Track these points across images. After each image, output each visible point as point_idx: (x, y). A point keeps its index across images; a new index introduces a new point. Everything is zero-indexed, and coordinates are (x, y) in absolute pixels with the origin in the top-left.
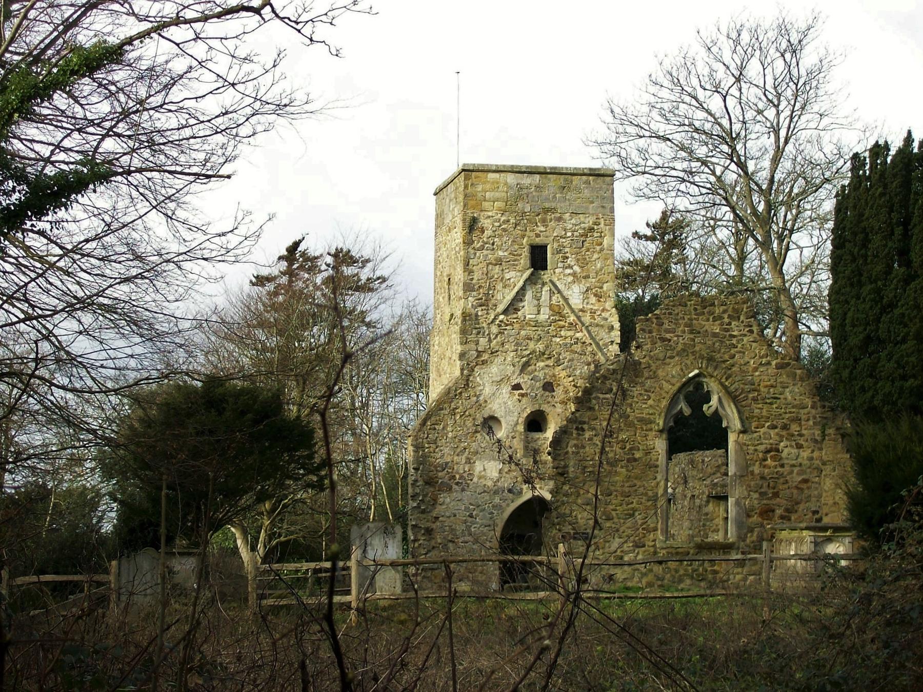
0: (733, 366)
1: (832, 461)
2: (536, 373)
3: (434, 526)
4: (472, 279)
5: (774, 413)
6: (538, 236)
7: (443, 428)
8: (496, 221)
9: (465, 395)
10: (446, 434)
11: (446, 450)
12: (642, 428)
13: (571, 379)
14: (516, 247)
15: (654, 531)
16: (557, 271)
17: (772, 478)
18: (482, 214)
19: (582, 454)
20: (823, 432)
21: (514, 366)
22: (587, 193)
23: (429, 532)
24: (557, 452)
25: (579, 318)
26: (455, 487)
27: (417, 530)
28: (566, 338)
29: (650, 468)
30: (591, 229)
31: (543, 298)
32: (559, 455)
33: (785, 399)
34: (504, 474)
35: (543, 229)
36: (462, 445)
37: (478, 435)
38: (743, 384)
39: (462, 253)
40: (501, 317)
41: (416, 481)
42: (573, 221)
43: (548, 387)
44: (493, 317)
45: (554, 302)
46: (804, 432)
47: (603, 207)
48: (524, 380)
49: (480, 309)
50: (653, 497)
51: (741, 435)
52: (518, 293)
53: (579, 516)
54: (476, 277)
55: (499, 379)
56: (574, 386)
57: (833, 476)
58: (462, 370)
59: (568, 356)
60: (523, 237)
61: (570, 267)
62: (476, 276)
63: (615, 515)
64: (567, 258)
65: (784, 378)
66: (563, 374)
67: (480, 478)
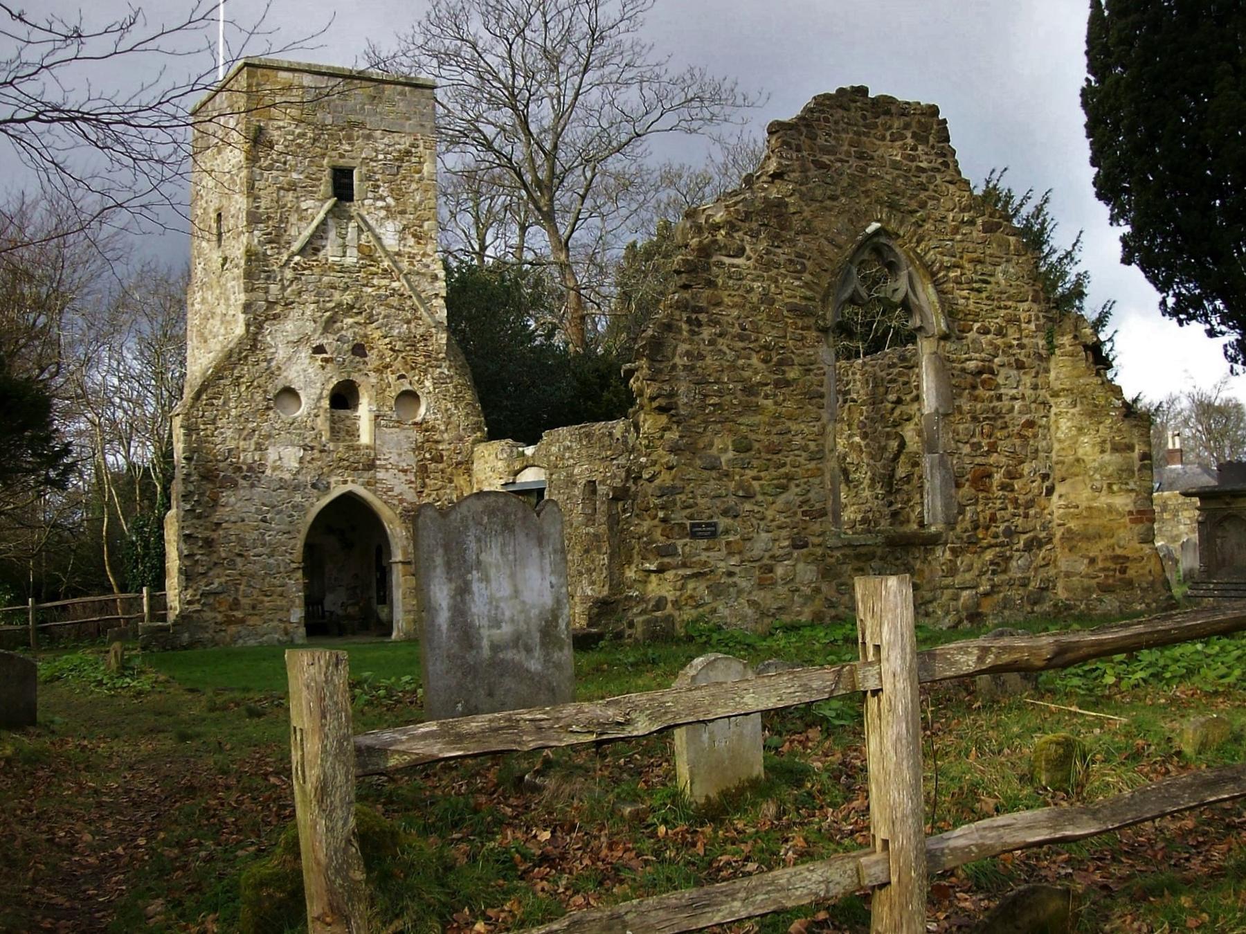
0: (924, 221)
1: (1070, 390)
2: (344, 333)
3: (215, 536)
4: (258, 208)
5: (985, 308)
6: (342, 156)
7: (225, 403)
8: (289, 133)
9: (251, 359)
10: (228, 411)
11: (229, 433)
12: (795, 323)
13: (387, 340)
14: (315, 168)
15: (821, 516)
16: (366, 202)
17: (987, 418)
18: (271, 123)
19: (700, 371)
20: (1050, 343)
21: (315, 322)
22: (402, 106)
23: (209, 543)
24: (657, 365)
25: (395, 262)
26: (241, 481)
27: (192, 540)
28: (380, 288)
29: (810, 399)
30: (408, 153)
31: (349, 236)
32: (660, 371)
33: (997, 283)
34: (306, 464)
35: (348, 148)
36: (250, 425)
37: (271, 413)
38: (941, 253)
39: (244, 173)
40: (297, 258)
41: (188, 475)
42: (386, 141)
43: (359, 350)
44: (285, 258)
45: (362, 242)
46: (1025, 341)
47: (422, 126)
48: (328, 341)
49: (269, 246)
50: (818, 452)
51: (942, 343)
52: (317, 227)
53: (699, 492)
54: (263, 205)
55: (295, 338)
56: (391, 349)
57: (1073, 415)
58: (248, 325)
59: (382, 310)
60: (323, 156)
61: (383, 198)
62: (263, 203)
63: (758, 489)
64: (379, 187)
65: (993, 249)
66: (377, 334)
67: (274, 469)
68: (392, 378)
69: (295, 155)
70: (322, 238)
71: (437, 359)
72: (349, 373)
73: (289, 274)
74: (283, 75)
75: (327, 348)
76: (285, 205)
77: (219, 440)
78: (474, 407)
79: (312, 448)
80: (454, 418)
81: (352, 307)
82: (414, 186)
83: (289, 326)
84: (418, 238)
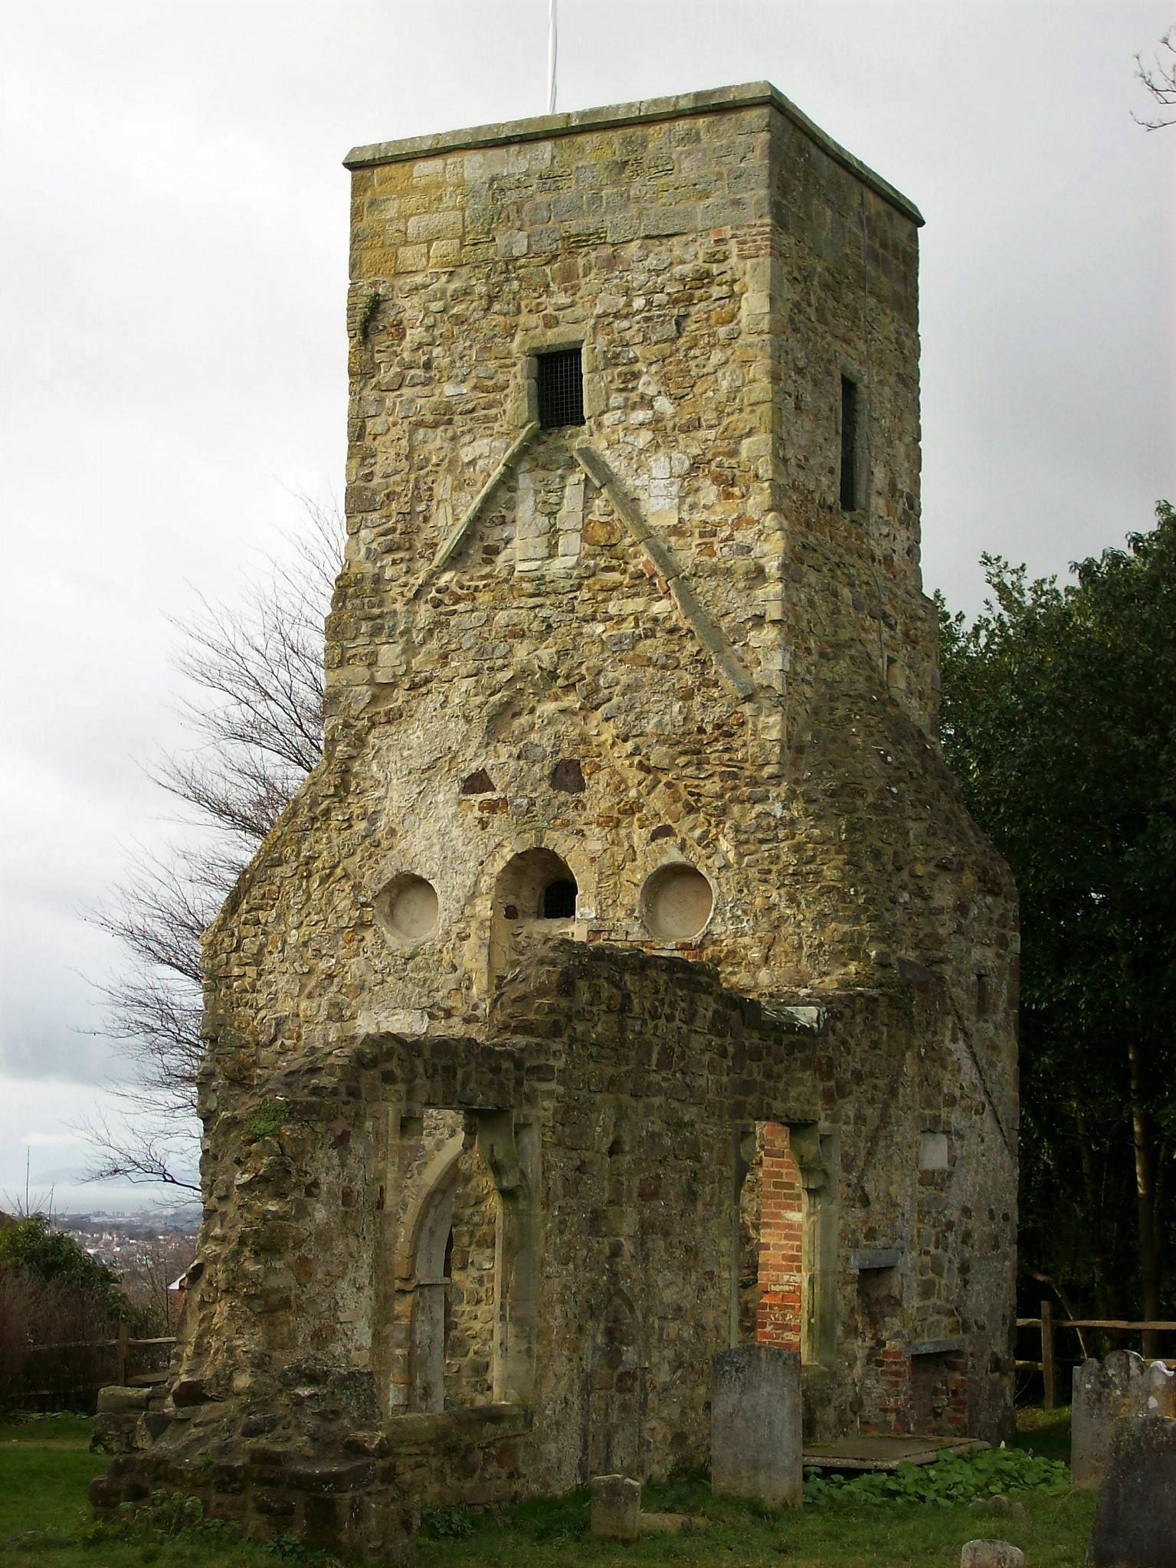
2: (534, 737)
4: (369, 477)
6: (551, 322)
9: (337, 816)
11: (282, 983)
13: (629, 746)
14: (492, 364)
18: (399, 282)
21: (468, 720)
28: (622, 619)
30: (703, 278)
36: (323, 965)
37: (369, 935)
42: (652, 262)
45: (595, 517)
47: (737, 203)
49: (388, 559)
56: (642, 766)
59: (622, 674)
60: (510, 333)
61: (647, 402)
62: (383, 463)
64: (636, 376)
68: (639, 836)
69: (449, 339)
70: (503, 521)
71: (754, 782)
72: (540, 831)
73: (424, 614)
74: (424, 169)
75: (494, 777)
76: (427, 460)
77: (262, 999)
78: (844, 897)
79: (448, 1014)
80: (788, 929)
81: (553, 676)
82: (717, 356)
83: (415, 735)
84: (727, 483)
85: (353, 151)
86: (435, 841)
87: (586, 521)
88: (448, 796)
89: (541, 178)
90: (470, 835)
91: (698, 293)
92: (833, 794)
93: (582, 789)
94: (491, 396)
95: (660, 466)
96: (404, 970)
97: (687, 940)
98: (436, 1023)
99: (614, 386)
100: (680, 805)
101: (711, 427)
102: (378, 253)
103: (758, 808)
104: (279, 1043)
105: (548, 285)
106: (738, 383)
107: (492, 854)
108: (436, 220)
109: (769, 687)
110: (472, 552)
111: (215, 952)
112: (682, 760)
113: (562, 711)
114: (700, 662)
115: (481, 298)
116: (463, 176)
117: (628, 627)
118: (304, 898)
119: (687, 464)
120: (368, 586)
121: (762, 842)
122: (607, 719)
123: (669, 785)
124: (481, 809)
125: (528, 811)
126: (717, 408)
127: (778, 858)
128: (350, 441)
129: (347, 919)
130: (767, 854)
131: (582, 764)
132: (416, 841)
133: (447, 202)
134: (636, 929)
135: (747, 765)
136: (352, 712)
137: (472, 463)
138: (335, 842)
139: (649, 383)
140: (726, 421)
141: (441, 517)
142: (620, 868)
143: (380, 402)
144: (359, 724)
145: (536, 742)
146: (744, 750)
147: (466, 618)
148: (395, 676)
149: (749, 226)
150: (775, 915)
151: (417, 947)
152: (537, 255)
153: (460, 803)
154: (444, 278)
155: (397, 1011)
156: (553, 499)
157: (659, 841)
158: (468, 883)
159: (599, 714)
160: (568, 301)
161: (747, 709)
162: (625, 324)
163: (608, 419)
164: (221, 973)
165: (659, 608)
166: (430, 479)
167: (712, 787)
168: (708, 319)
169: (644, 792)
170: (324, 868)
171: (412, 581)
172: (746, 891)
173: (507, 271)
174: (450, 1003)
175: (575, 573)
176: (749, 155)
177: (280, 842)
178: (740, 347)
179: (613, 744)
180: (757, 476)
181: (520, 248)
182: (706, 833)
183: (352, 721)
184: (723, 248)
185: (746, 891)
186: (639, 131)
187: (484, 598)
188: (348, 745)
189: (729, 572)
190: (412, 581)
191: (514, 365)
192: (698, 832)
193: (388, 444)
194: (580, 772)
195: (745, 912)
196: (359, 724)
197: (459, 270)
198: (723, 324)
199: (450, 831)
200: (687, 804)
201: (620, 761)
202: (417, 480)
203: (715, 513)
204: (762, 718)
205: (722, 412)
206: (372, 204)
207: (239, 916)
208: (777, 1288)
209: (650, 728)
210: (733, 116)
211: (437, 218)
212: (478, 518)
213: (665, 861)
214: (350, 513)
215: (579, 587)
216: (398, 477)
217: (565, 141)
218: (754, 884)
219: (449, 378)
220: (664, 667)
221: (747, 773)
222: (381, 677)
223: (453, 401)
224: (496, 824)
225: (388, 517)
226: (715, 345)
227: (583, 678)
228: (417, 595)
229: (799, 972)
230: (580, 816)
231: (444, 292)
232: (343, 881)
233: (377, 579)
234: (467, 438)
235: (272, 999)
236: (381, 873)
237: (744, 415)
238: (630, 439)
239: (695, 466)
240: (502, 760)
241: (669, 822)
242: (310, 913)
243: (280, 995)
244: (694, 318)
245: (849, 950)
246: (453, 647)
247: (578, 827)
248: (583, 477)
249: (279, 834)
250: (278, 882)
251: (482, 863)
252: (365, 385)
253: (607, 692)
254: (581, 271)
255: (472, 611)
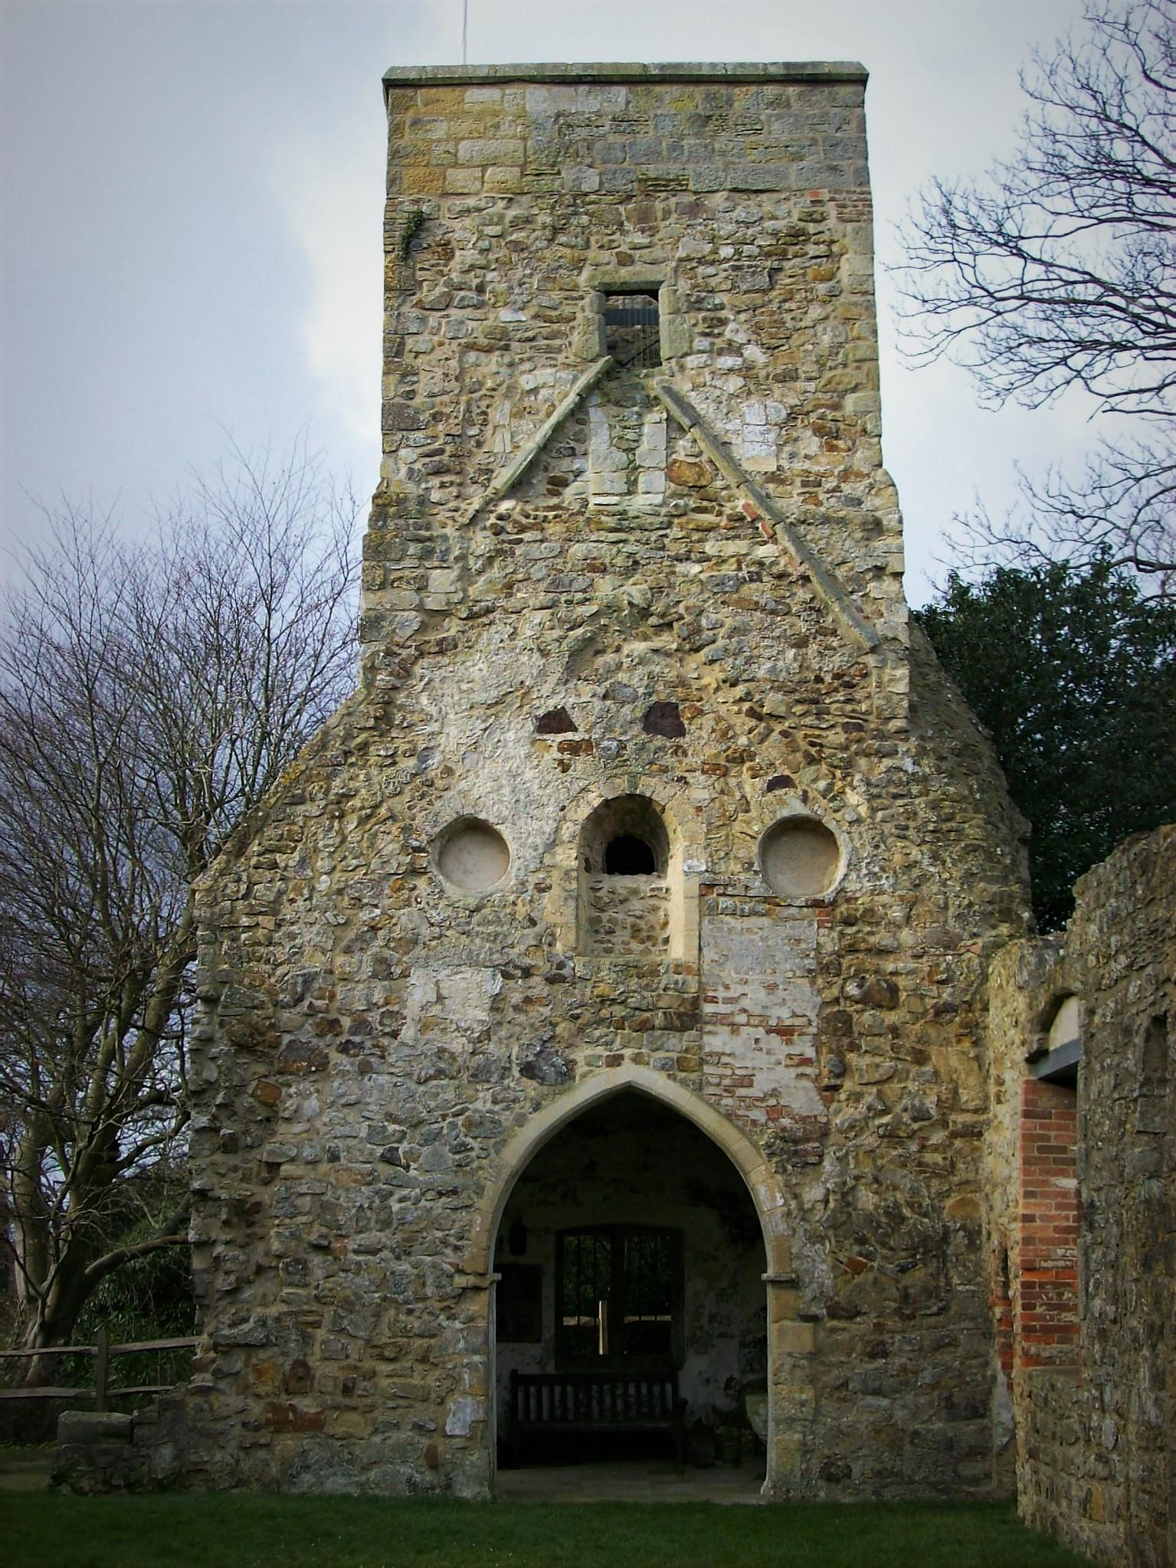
2: (622, 677)
4: (410, 395)
6: (625, 260)
9: (378, 751)
11: (309, 935)
13: (740, 690)
14: (556, 296)
18: (447, 203)
21: (544, 653)
30: (797, 236)
36: (364, 915)
37: (422, 883)
42: (739, 213)
45: (680, 456)
47: (833, 169)
49: (435, 481)
56: (751, 713)
59: (728, 617)
60: (578, 265)
61: (735, 349)
64: (723, 322)
69: (505, 265)
70: (573, 453)
71: (881, 736)
72: (634, 778)
73: (482, 542)
74: (475, 96)
75: (576, 717)
76: (481, 384)
77: (281, 954)
78: (990, 856)
79: (527, 972)
80: (931, 888)
81: (645, 613)
85: (392, 69)
86: (505, 782)
87: (670, 460)
88: (520, 734)
89: (614, 119)
90: (548, 778)
91: (792, 250)
92: (958, 754)
93: (682, 732)
94: (555, 326)
95: (754, 412)
96: (469, 923)
97: (819, 897)
98: (511, 983)
99: (698, 330)
100: (799, 755)
101: (810, 379)
102: (421, 171)
103: (887, 762)
104: (306, 1003)
105: (622, 224)
106: (841, 339)
107: (575, 799)
108: (492, 146)
109: (895, 639)
110: (535, 481)
111: (215, 898)
112: (799, 709)
113: (655, 651)
114: (815, 609)
115: (544, 228)
116: (524, 108)
117: (729, 569)
118: (338, 839)
119: (784, 414)
120: (412, 507)
121: (896, 797)
122: (712, 662)
123: (784, 734)
124: (561, 750)
125: (618, 755)
126: (817, 362)
127: (915, 814)
128: (386, 357)
129: (395, 865)
130: (901, 810)
131: (681, 707)
132: (480, 781)
133: (505, 130)
134: (757, 884)
135: (871, 718)
136: (396, 639)
137: (534, 391)
138: (375, 780)
139: (737, 331)
140: (828, 375)
141: (498, 443)
142: (732, 819)
143: (423, 320)
144: (405, 653)
145: (625, 681)
146: (868, 702)
147: (530, 546)
148: (448, 603)
149: (848, 192)
150: (915, 873)
151: (483, 898)
152: (609, 193)
153: (533, 742)
154: (501, 204)
155: (463, 969)
156: (631, 435)
157: (777, 792)
158: (547, 829)
159: (702, 656)
160: (645, 241)
161: (871, 660)
162: (711, 270)
163: (691, 361)
164: (224, 922)
165: (763, 552)
166: (484, 403)
167: (835, 737)
168: (804, 275)
169: (755, 741)
170: (362, 808)
171: (463, 506)
172: (883, 847)
173: (574, 205)
174: (527, 961)
175: (664, 511)
176: (845, 127)
177: (303, 777)
178: (843, 304)
179: (717, 689)
180: (864, 431)
181: (591, 181)
182: (831, 786)
183: (395, 649)
184: (821, 209)
185: (883, 847)
186: (723, 90)
187: (554, 529)
188: (391, 674)
189: (843, 522)
190: (463, 506)
191: (582, 298)
192: (822, 784)
193: (434, 363)
194: (678, 717)
195: (883, 869)
196: (405, 653)
197: (518, 198)
198: (822, 281)
199: (523, 773)
200: (807, 755)
201: (725, 707)
202: (468, 403)
203: (818, 463)
204: (888, 671)
205: (823, 365)
206: (415, 122)
207: (248, 859)
208: (1049, 1264)
209: (761, 673)
210: (826, 89)
211: (493, 145)
212: (544, 448)
213: (785, 813)
214: (387, 431)
215: (670, 525)
216: (446, 398)
217: (640, 89)
218: (890, 840)
219: (506, 304)
220: (773, 612)
221: (872, 726)
222: (431, 604)
223: (511, 327)
224: (580, 767)
225: (435, 437)
226: (812, 300)
227: (681, 618)
228: (474, 520)
229: (947, 933)
230: (680, 762)
231: (502, 217)
232: (389, 822)
233: (423, 501)
234: (527, 366)
235: (295, 953)
236: (437, 815)
237: (849, 370)
238: (718, 383)
239: (792, 417)
240: (584, 699)
241: (787, 773)
242: (345, 857)
243: (308, 949)
244: (789, 273)
245: (1000, 912)
246: (520, 577)
247: (679, 774)
248: (665, 416)
249: (303, 768)
250: (300, 821)
251: (563, 809)
252: (404, 301)
253: (711, 633)
254: (659, 215)
255: (542, 541)
